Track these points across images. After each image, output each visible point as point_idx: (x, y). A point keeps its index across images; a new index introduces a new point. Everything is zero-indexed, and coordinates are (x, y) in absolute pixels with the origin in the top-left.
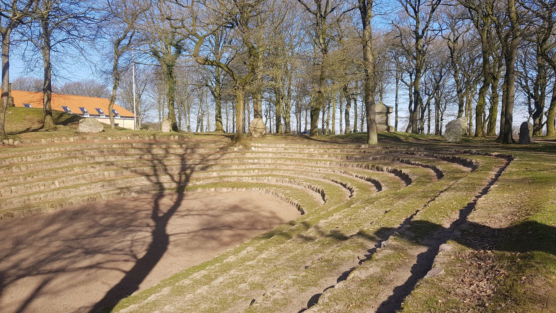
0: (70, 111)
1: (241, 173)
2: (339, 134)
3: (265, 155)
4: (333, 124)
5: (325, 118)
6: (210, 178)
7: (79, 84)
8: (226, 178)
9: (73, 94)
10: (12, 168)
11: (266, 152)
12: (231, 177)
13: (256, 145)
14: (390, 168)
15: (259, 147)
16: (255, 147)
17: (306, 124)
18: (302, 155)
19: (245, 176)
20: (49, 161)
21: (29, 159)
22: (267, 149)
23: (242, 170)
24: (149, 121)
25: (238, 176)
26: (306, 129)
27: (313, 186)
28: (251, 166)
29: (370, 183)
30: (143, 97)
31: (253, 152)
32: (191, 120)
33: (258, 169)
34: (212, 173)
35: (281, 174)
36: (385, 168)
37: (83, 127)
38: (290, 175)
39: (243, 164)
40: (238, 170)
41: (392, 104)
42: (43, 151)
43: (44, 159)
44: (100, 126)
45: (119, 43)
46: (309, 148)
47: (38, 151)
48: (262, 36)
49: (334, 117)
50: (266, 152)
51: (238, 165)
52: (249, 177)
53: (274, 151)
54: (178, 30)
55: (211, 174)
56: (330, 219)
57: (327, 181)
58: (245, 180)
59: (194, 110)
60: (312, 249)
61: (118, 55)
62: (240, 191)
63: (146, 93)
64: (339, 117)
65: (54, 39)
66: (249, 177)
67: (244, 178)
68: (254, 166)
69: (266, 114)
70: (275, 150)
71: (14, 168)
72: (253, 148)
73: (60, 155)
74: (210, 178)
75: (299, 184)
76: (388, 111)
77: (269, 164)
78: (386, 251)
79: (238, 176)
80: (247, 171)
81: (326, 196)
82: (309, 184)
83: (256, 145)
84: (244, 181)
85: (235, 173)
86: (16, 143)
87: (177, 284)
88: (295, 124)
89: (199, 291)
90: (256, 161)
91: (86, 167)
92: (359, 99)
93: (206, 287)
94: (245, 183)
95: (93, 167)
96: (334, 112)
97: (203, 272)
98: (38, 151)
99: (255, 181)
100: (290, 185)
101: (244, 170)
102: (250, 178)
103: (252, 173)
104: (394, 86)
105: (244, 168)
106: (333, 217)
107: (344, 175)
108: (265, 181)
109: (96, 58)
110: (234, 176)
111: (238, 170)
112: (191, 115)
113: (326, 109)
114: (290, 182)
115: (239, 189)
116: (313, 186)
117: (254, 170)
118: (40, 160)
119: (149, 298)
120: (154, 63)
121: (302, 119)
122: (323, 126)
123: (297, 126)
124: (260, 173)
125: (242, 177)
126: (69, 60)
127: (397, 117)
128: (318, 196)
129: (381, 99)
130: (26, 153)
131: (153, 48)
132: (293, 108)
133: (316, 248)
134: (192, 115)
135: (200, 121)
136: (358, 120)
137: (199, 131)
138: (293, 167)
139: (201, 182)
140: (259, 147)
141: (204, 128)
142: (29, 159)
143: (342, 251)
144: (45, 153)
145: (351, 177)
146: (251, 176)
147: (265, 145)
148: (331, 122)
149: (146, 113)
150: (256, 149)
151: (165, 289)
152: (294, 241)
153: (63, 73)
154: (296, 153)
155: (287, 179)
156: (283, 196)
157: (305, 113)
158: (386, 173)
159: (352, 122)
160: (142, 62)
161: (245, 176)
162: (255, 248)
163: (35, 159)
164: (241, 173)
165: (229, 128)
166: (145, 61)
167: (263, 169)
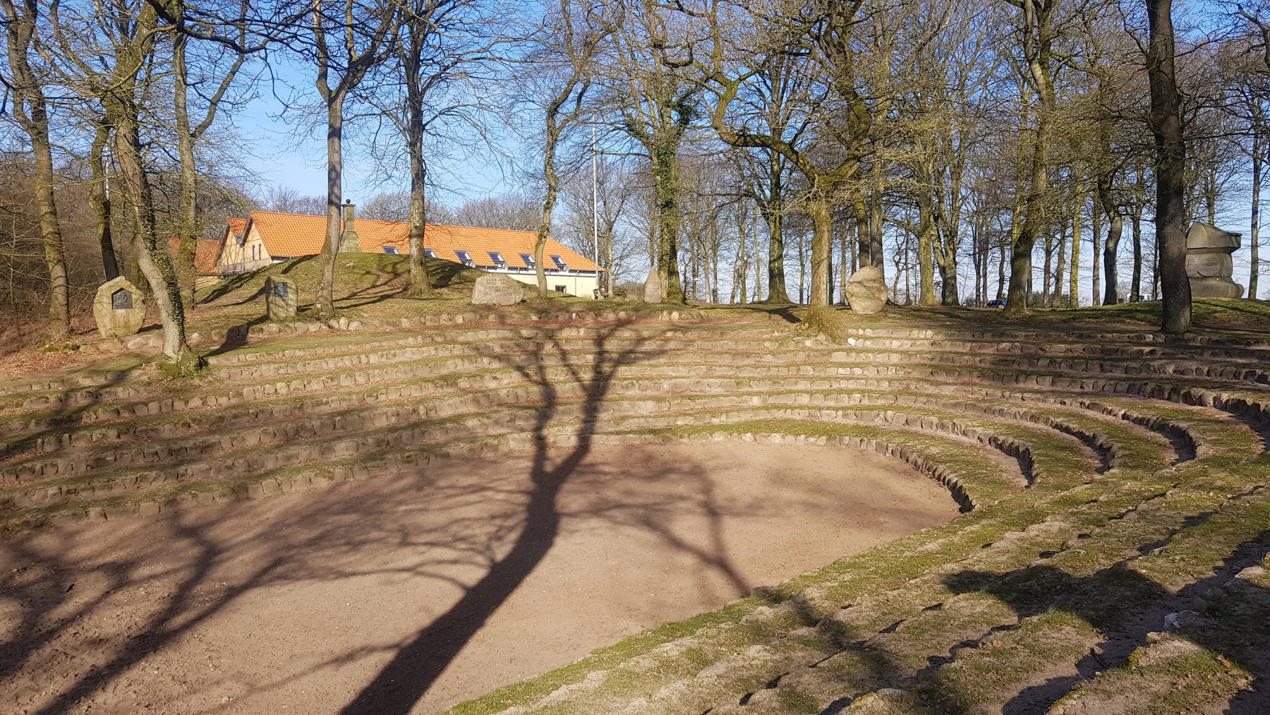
0: (470, 261)
1: (819, 401)
2: (1090, 304)
3: (881, 358)
4: (1073, 281)
5: (1053, 266)
6: (745, 409)
7: (491, 204)
8: (781, 412)
9: (480, 225)
10: (338, 377)
11: (884, 351)
12: (792, 408)
13: (861, 332)
14: (1225, 396)
15: (866, 338)
16: (857, 337)
17: (1001, 281)
18: (978, 359)
19: (828, 408)
20: (409, 363)
21: (373, 359)
22: (887, 342)
23: (822, 392)
24: (630, 279)
25: (809, 408)
26: (1000, 294)
27: (1001, 438)
28: (843, 385)
29: (1161, 438)
30: (619, 227)
31: (850, 350)
32: (719, 276)
33: (862, 392)
34: (748, 398)
35: (918, 405)
36: (1210, 396)
37: (482, 292)
38: (943, 410)
39: (824, 379)
40: (811, 393)
41: (1244, 228)
42: (401, 342)
43: (402, 359)
44: (516, 292)
45: (556, 110)
46: (999, 343)
47: (392, 344)
48: (882, 67)
49: (1074, 264)
50: (884, 351)
51: (812, 380)
52: (836, 409)
53: (905, 348)
54: (679, 71)
55: (746, 401)
56: (1034, 530)
57: (1041, 426)
58: (828, 417)
59: (726, 253)
60: (968, 612)
61: (553, 136)
62: (813, 444)
63: (624, 218)
64: (1042, 265)
65: (431, 108)
66: (836, 409)
67: (824, 412)
68: (851, 385)
69: (897, 259)
70: (907, 345)
71: (342, 377)
72: (851, 341)
73: (433, 352)
74: (745, 409)
75: (965, 434)
76: (1231, 243)
77: (890, 381)
78: (1177, 643)
79: (809, 408)
80: (833, 396)
81: (1036, 466)
82: (991, 432)
83: (861, 332)
84: (825, 419)
85: (804, 399)
86: (354, 326)
87: (621, 666)
88: (973, 283)
89: (664, 692)
90: (858, 371)
91: (482, 377)
92: (1147, 215)
93: (681, 685)
94: (827, 424)
95: (495, 378)
96: (1076, 251)
97: (688, 642)
98: (392, 344)
99: (851, 421)
100: (940, 433)
101: (826, 394)
102: (840, 413)
103: (845, 401)
104: (1246, 180)
105: (827, 387)
106: (1043, 526)
107: (1090, 413)
108: (879, 422)
109: (512, 144)
110: (801, 407)
111: (811, 393)
112: (720, 265)
113: (1055, 243)
114: (943, 427)
115: (812, 440)
116: (1001, 438)
117: (850, 392)
118: (394, 361)
119: (554, 694)
120: (636, 151)
121: (989, 268)
122: (1047, 286)
123: (978, 290)
124: (866, 402)
125: (820, 409)
126: (458, 152)
127: (1255, 261)
128: (1011, 466)
129: (1211, 215)
130: (368, 347)
131: (629, 115)
132: (967, 244)
133: (979, 609)
134: (722, 265)
135: (740, 277)
136: (1143, 269)
137: (737, 299)
138: (952, 388)
139: (723, 418)
140: (866, 338)
141: (749, 294)
142: (373, 359)
143: (1046, 629)
144: (403, 347)
145: (1110, 418)
146: (843, 408)
147: (882, 333)
148: (1066, 276)
149: (625, 262)
150: (860, 344)
151: (592, 675)
152: (925, 582)
153: (446, 179)
154: (964, 354)
155: (935, 419)
156: (920, 461)
157: (998, 254)
158: (1211, 411)
159: (1124, 276)
160: (611, 150)
161: (828, 408)
162: (824, 593)
163: (384, 359)
164: (819, 401)
165: (805, 293)
166: (616, 148)
167: (874, 392)
